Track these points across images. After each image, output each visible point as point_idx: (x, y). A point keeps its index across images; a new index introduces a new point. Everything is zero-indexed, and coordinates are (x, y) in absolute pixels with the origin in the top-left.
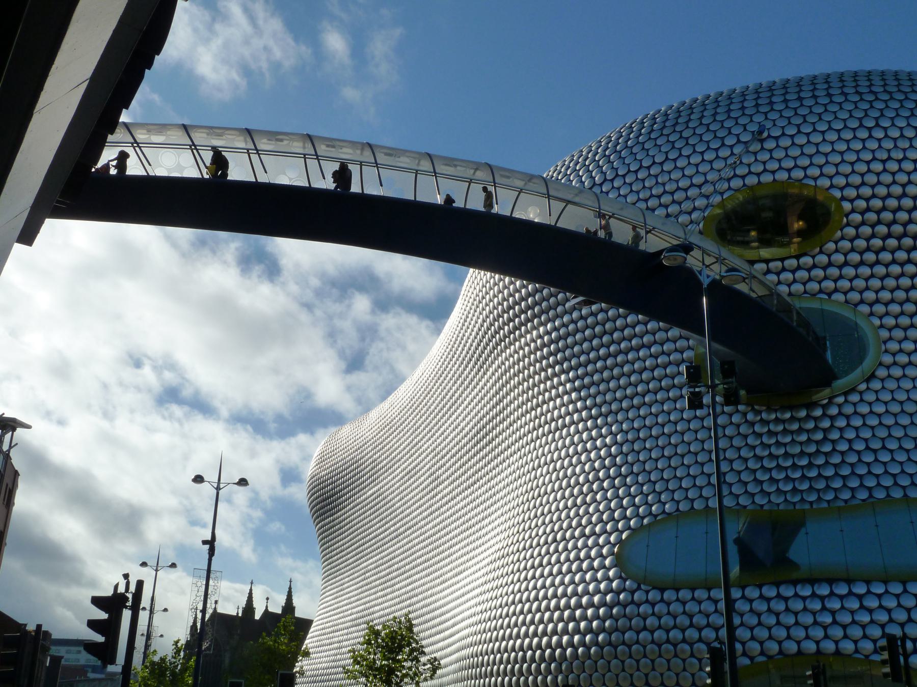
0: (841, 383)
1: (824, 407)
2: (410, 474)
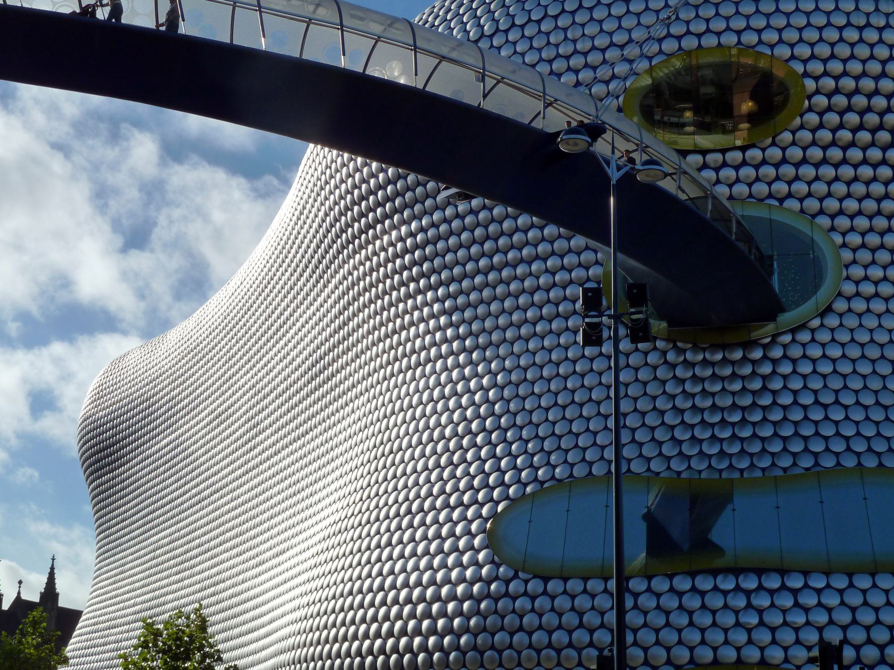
0: (787, 318)
2: (219, 418)
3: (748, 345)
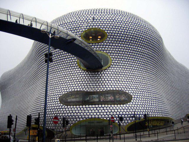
0: (104, 68)
1: (100, 72)
2: (20, 81)
3: (98, 72)
